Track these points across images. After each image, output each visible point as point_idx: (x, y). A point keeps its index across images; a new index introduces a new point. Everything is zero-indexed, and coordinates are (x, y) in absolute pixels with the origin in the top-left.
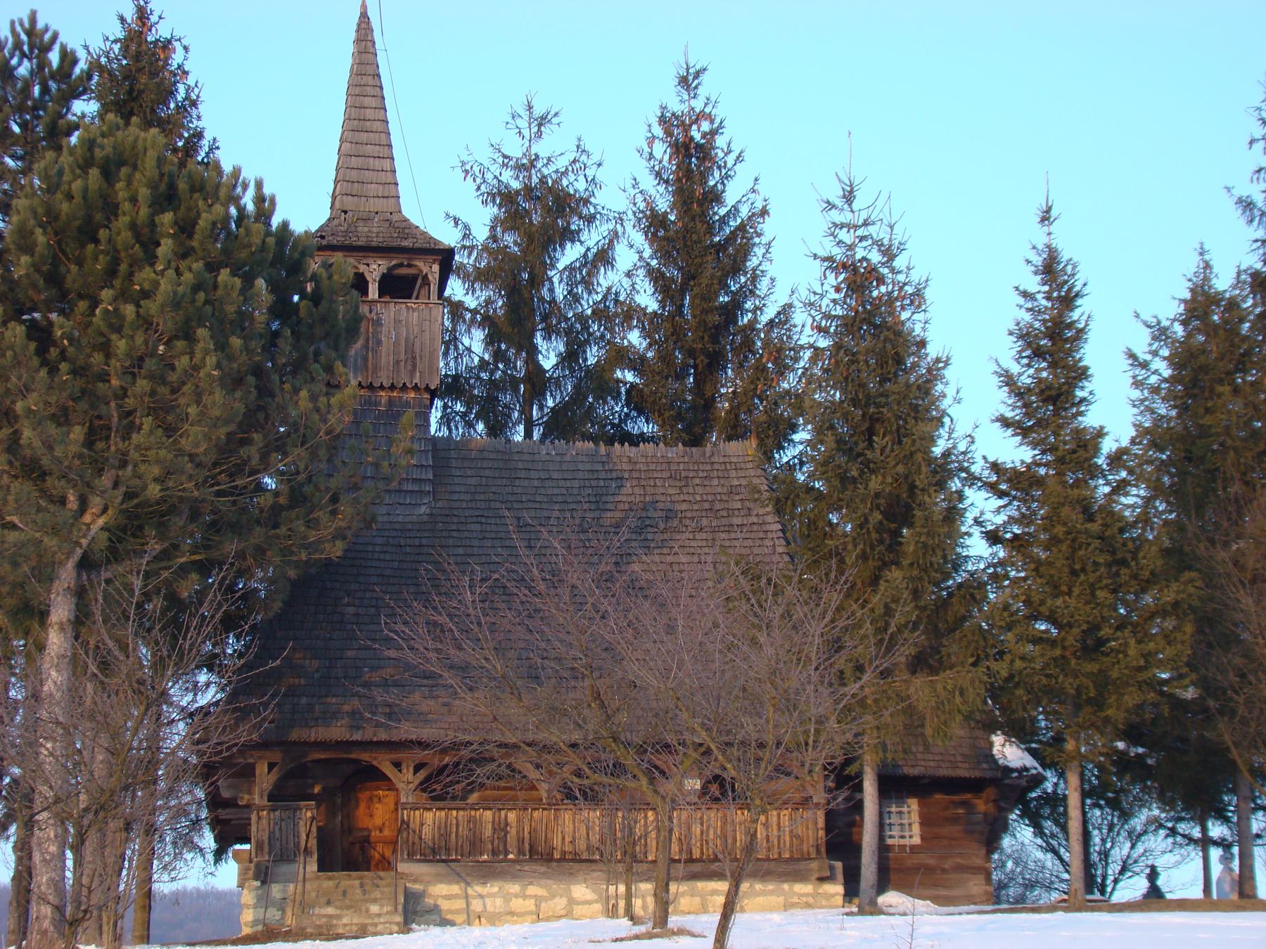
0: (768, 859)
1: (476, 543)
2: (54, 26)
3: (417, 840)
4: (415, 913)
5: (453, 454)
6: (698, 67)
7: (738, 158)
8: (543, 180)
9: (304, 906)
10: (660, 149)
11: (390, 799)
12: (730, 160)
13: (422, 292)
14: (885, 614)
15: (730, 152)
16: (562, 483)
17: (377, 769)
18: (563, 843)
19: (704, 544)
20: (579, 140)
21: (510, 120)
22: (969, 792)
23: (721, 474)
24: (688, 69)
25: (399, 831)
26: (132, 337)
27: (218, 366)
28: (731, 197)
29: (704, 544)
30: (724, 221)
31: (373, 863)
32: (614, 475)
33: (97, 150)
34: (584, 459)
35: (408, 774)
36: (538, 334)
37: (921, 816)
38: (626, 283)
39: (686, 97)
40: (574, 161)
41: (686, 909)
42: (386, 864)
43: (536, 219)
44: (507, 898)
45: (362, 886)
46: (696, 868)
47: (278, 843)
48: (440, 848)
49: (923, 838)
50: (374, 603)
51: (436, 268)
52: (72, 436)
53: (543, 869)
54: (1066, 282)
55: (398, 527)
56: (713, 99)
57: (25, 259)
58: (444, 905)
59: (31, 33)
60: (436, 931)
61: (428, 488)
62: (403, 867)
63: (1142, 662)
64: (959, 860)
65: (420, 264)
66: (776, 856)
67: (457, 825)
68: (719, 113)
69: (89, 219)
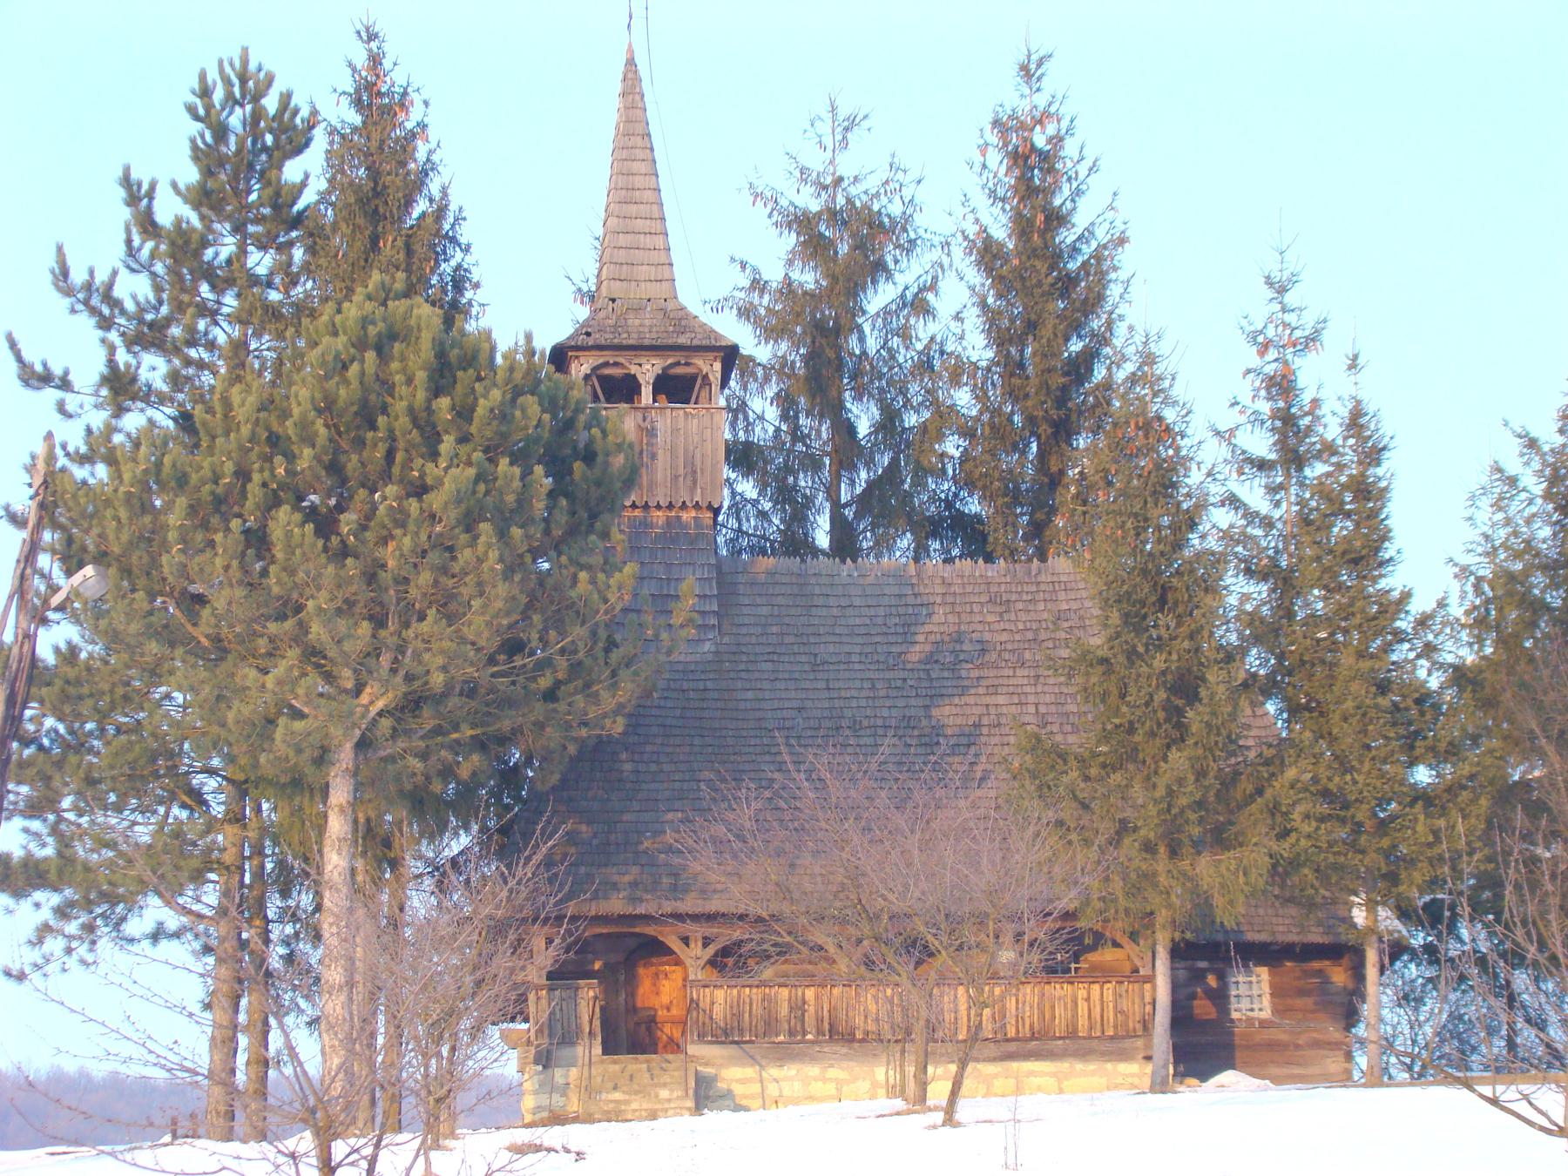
0: (1090, 1037)
1: (766, 685)
2: (267, 67)
4: (707, 1098)
5: (741, 579)
6: (1042, 53)
8: (849, 201)
9: (589, 1091)
10: (995, 159)
11: (676, 973)
12: (1083, 169)
13: (703, 394)
16: (866, 611)
17: (663, 943)
20: (893, 156)
21: (808, 127)
23: (1047, 596)
24: (1029, 56)
25: (688, 1011)
26: (417, 533)
27: (501, 560)
28: (1080, 220)
30: (1075, 250)
31: (660, 1046)
34: (891, 580)
37: (1272, 985)
38: (955, 327)
39: (1027, 91)
40: (887, 182)
42: (675, 1047)
43: (843, 249)
46: (1012, 1047)
50: (655, 757)
51: (718, 366)
53: (844, 1050)
55: (680, 667)
57: (307, 452)
58: (738, 1089)
61: (713, 621)
62: (692, 1049)
63: (1431, 839)
64: (1315, 1035)
68: (1066, 111)
69: (364, 403)
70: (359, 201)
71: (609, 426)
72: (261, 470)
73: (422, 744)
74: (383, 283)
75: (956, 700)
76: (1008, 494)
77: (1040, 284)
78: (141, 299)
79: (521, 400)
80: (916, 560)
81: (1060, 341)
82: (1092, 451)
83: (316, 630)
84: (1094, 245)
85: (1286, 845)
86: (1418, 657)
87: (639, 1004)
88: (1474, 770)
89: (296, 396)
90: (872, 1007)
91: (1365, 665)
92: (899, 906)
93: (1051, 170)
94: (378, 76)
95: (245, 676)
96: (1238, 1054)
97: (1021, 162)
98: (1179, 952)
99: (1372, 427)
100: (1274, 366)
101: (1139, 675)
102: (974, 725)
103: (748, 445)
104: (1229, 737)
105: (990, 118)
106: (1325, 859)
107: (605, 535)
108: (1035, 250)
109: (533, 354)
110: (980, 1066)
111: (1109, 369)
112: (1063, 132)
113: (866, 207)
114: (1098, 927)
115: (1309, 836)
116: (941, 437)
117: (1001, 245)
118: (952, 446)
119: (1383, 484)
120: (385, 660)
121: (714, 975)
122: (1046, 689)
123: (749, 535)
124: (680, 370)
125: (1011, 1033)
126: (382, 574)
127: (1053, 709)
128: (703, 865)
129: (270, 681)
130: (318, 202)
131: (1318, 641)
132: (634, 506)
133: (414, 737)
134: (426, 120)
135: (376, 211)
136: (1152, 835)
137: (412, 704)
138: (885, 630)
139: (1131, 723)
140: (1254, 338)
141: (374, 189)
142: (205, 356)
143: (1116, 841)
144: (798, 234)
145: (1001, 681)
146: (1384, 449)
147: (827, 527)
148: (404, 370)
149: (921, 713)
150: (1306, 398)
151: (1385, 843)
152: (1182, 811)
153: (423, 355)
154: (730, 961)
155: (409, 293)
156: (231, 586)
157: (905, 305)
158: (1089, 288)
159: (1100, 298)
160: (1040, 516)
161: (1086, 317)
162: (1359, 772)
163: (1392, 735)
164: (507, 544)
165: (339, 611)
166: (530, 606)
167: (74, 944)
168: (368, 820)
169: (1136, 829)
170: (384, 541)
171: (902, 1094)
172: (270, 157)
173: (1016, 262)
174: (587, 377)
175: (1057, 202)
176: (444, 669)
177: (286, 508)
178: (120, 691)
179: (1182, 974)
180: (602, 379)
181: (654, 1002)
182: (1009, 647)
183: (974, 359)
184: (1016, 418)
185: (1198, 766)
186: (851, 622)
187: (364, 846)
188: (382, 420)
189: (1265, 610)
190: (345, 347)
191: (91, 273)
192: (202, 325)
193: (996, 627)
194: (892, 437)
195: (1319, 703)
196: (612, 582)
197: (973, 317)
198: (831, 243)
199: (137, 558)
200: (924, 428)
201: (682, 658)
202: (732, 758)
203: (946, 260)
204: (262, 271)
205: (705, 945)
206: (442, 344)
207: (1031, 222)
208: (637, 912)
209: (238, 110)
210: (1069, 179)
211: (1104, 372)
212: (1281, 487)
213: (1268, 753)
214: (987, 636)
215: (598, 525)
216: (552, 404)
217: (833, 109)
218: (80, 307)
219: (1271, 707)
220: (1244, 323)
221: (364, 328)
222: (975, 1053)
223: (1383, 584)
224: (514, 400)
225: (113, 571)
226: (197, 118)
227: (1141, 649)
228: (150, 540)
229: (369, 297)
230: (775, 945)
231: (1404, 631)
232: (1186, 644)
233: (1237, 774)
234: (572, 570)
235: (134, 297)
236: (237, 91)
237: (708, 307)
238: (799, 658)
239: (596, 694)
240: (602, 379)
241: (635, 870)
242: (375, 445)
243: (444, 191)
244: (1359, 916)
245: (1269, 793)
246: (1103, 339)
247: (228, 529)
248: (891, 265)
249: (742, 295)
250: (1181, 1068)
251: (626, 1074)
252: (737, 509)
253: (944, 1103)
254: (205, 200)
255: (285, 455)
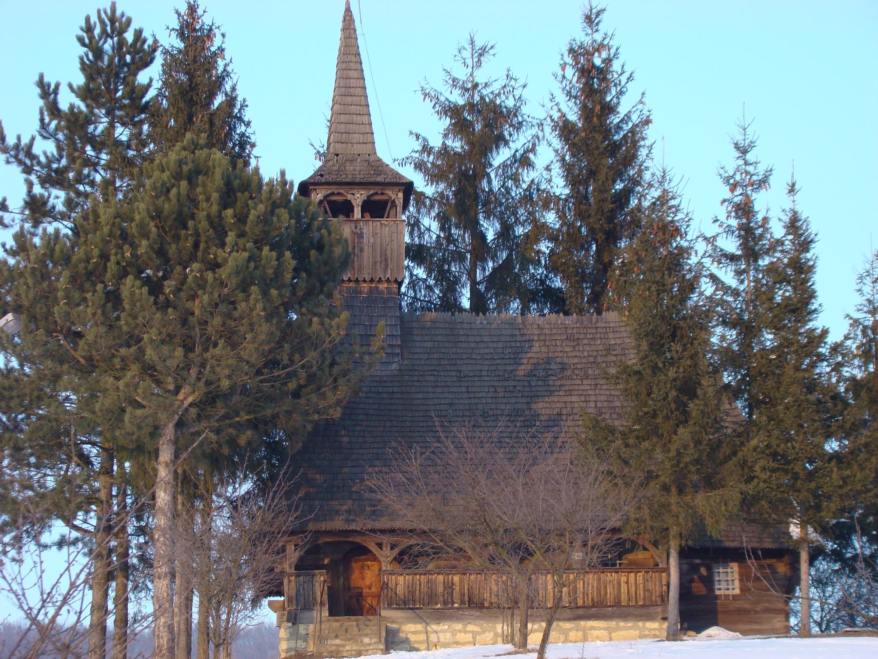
0: (629, 606)
1: (430, 390)
2: (128, 14)
3: (393, 595)
4: (393, 643)
5: (415, 325)
6: (599, 8)
7: (628, 79)
8: (482, 98)
10: (570, 72)
11: (375, 566)
12: (624, 79)
13: (392, 212)
14: (677, 455)
15: (623, 72)
16: (491, 345)
18: (491, 596)
19: (589, 388)
20: (509, 70)
21: (457, 53)
22: (773, 558)
23: (602, 336)
24: (591, 10)
25: (382, 589)
26: (212, 293)
27: (264, 309)
28: (623, 110)
29: (589, 388)
30: (618, 127)
31: (365, 610)
32: (527, 338)
33: (184, 166)
34: (507, 326)
35: (387, 551)
36: (481, 216)
37: (740, 574)
39: (590, 31)
40: (505, 86)
41: (573, 639)
42: (373, 611)
43: (478, 127)
44: (454, 633)
45: (357, 625)
46: (581, 612)
47: (302, 598)
48: (409, 600)
49: (741, 590)
51: (401, 195)
52: (176, 353)
53: (478, 614)
54: (803, 234)
55: (377, 379)
56: (610, 34)
57: (144, 243)
58: (412, 638)
59: (113, 20)
60: (403, 654)
61: (398, 351)
62: (384, 613)
63: (841, 483)
64: (766, 605)
65: (390, 193)
66: (634, 604)
67: (420, 585)
68: (614, 43)
69: (180, 213)
70: (181, 93)
71: (332, 229)
72: (116, 254)
73: (216, 424)
74: (192, 139)
75: (546, 399)
76: (576, 275)
77: (597, 148)
78: (49, 155)
79: (277, 211)
80: (523, 314)
81: (610, 182)
82: (629, 248)
83: (150, 353)
84: (630, 125)
85: (751, 487)
86: (832, 370)
87: (352, 585)
88: (868, 440)
89: (138, 208)
90: (495, 588)
91: (800, 375)
92: (511, 524)
93: (604, 79)
94: (194, 19)
95: (106, 382)
96: (720, 616)
97: (586, 74)
98: (684, 554)
99: (804, 227)
100: (740, 198)
101: (659, 382)
102: (557, 414)
103: (421, 247)
104: (715, 419)
105: (567, 47)
106: (776, 495)
107: (330, 296)
108: (595, 127)
109: (286, 184)
110: (561, 624)
111: (640, 200)
112: (612, 55)
113: (492, 101)
114: (634, 538)
115: (765, 481)
116: (537, 241)
117: (574, 125)
118: (545, 246)
119: (811, 263)
120: (194, 372)
121: (398, 568)
122: (602, 392)
123: (421, 301)
124: (377, 198)
125: (580, 603)
126: (191, 318)
127: (606, 404)
128: (389, 498)
129: (121, 384)
130: (157, 96)
131: (771, 360)
132: (349, 280)
133: (212, 420)
134: (224, 46)
135: (191, 99)
136: (667, 480)
137: (210, 399)
138: (502, 356)
139: (655, 411)
140: (728, 181)
141: (190, 86)
142: (88, 189)
143: (644, 484)
144: (451, 119)
145: (573, 387)
146: (812, 241)
147: (468, 295)
148: (204, 193)
149: (525, 406)
150: (760, 217)
151: (813, 485)
152: (686, 465)
153: (216, 183)
154: (406, 558)
155: (210, 145)
156: (97, 326)
157: (516, 161)
158: (627, 150)
159: (634, 156)
160: (597, 289)
161: (626, 168)
162: (796, 441)
163: (817, 418)
164: (268, 300)
165: (163, 342)
166: (283, 338)
167: (8, 549)
168: (184, 472)
169: (657, 476)
170: (193, 297)
171: (512, 641)
172: (129, 69)
173: (583, 134)
174: (321, 202)
175: (608, 99)
176: (229, 377)
177: (130, 278)
178: (36, 393)
179: (685, 567)
180: (330, 202)
181: (360, 583)
182: (579, 366)
183: (557, 194)
184: (583, 229)
185: (696, 438)
186: (482, 351)
187: (182, 487)
188: (191, 223)
189: (735, 348)
190: (168, 178)
191: (19, 138)
192: (86, 171)
193: (571, 354)
194: (508, 241)
195: (770, 399)
196: (333, 323)
197: (557, 169)
198: (471, 124)
199: (40, 309)
200: (527, 235)
201: (379, 373)
202: (409, 434)
203: (540, 134)
204: (124, 138)
205: (392, 548)
206: (228, 177)
207: (592, 110)
208: (351, 528)
209: (110, 41)
210: (615, 85)
211: (636, 201)
212: (744, 271)
213: (741, 429)
214: (565, 360)
215: (325, 289)
216: (296, 214)
217: (472, 43)
218: (12, 160)
219: (739, 404)
220: (722, 171)
221: (180, 166)
222: (557, 615)
223: (810, 325)
224: (272, 213)
225: (23, 317)
226: (83, 44)
227: (660, 365)
228: (48, 297)
229: (184, 149)
230: (433, 548)
231: (824, 355)
232: (689, 362)
233: (720, 442)
234: (309, 316)
235: (45, 153)
236: (109, 29)
237: (397, 163)
238: (449, 373)
239: (324, 394)
240: (330, 202)
241: (350, 502)
242: (187, 239)
243: (234, 89)
244: (795, 531)
245: (740, 454)
246: (636, 182)
247: (95, 291)
248: (508, 137)
249: (417, 155)
250: (686, 625)
251: (344, 628)
252: (414, 283)
253: (538, 647)
254: (88, 94)
255: (131, 245)
